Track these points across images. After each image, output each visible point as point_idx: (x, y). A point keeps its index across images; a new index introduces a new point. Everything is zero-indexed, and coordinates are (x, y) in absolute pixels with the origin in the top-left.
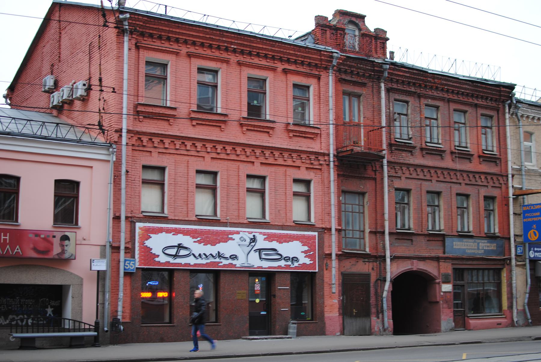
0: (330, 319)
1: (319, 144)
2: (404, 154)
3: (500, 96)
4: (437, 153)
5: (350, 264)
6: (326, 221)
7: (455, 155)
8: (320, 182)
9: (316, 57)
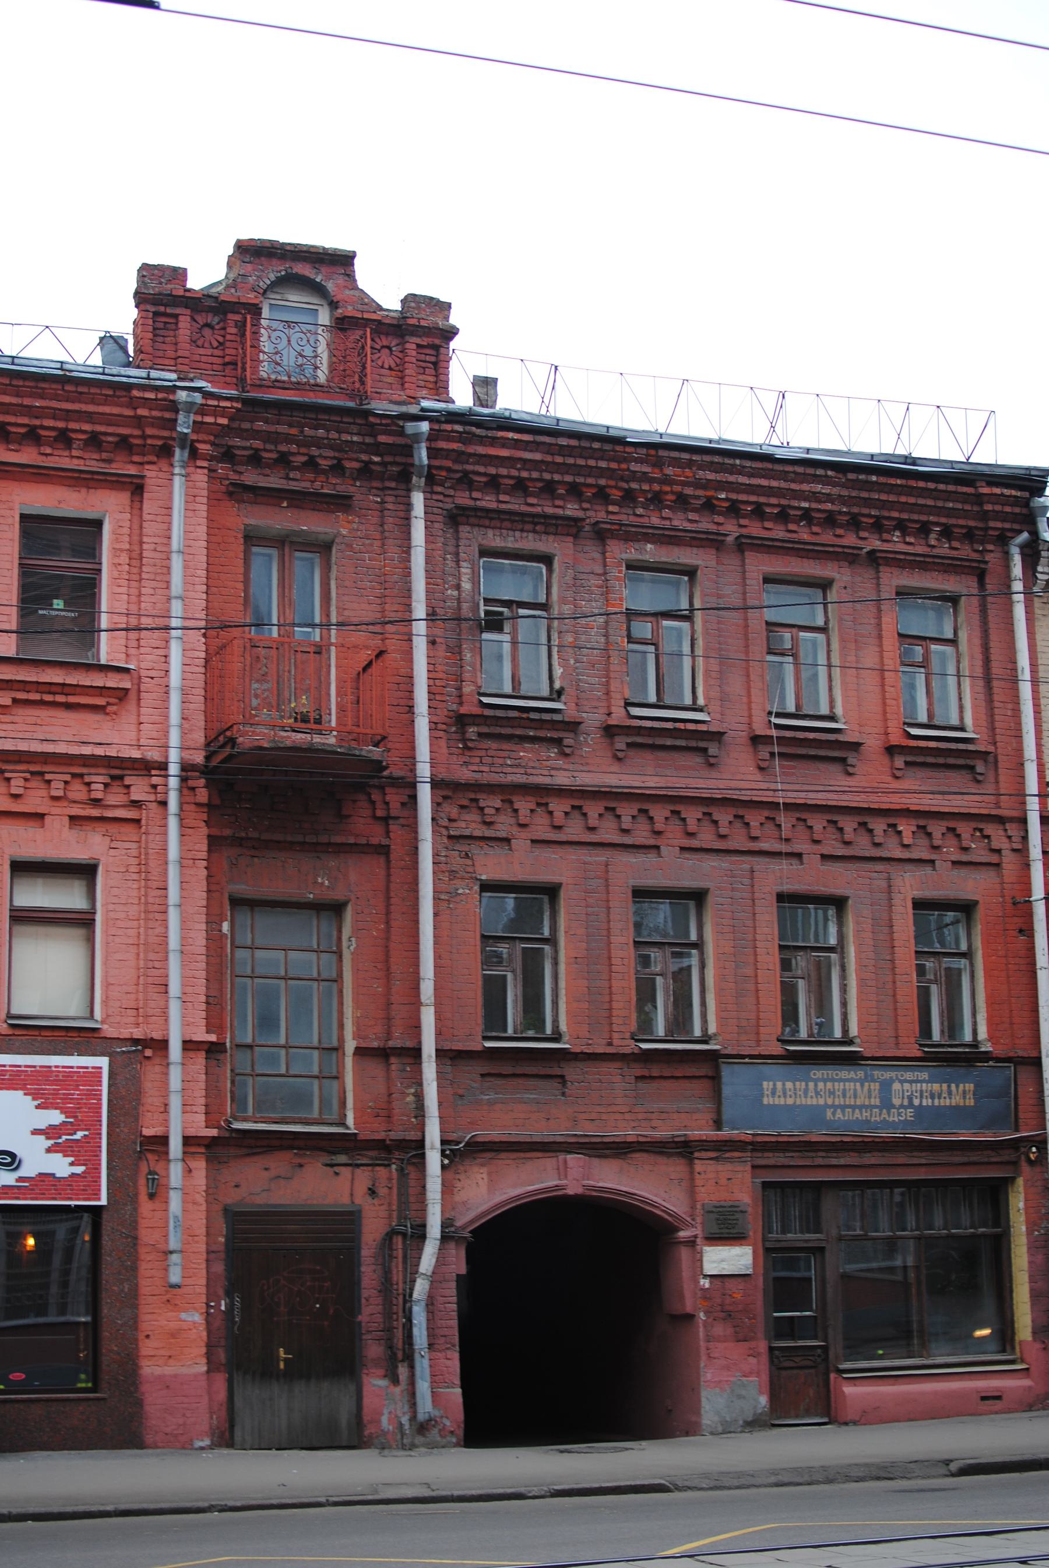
0: (166, 1384)
1: (133, 727)
2: (525, 753)
3: (985, 516)
4: (682, 743)
5: (266, 1174)
6: (151, 1012)
7: (769, 749)
8: (133, 869)
9: (116, 410)
